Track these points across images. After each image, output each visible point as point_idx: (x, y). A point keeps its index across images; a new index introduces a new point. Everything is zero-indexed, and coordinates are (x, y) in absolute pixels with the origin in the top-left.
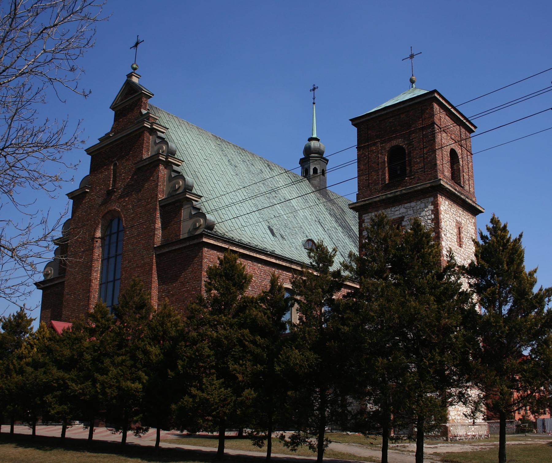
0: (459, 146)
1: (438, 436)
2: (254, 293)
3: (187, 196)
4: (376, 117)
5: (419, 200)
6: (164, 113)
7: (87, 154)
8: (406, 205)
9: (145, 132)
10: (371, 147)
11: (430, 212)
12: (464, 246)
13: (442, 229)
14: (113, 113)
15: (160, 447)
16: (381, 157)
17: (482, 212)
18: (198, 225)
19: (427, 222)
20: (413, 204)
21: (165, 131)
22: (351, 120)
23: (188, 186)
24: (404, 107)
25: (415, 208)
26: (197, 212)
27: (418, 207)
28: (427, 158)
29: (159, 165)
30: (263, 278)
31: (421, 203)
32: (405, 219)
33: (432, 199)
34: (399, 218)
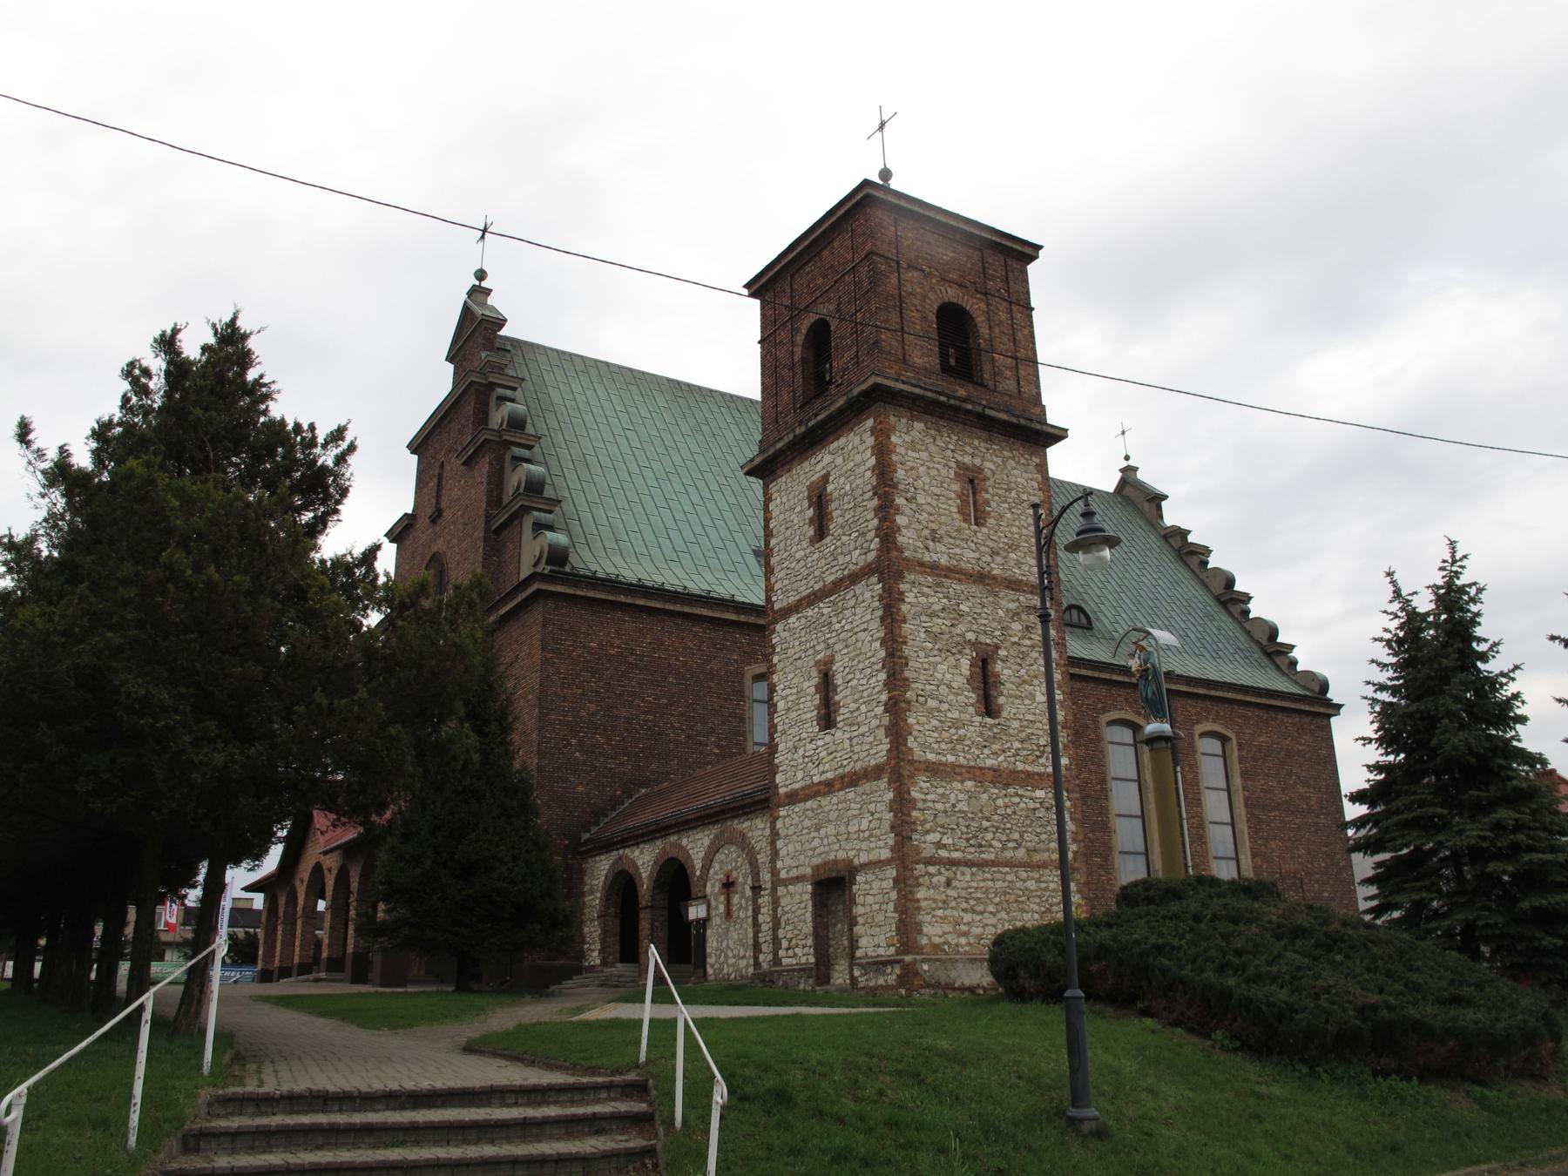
0: (978, 296)
2: (682, 689)
4: (784, 266)
5: (852, 430)
8: (833, 446)
12: (991, 521)
13: (895, 487)
20: (842, 441)
27: (850, 447)
32: (831, 478)
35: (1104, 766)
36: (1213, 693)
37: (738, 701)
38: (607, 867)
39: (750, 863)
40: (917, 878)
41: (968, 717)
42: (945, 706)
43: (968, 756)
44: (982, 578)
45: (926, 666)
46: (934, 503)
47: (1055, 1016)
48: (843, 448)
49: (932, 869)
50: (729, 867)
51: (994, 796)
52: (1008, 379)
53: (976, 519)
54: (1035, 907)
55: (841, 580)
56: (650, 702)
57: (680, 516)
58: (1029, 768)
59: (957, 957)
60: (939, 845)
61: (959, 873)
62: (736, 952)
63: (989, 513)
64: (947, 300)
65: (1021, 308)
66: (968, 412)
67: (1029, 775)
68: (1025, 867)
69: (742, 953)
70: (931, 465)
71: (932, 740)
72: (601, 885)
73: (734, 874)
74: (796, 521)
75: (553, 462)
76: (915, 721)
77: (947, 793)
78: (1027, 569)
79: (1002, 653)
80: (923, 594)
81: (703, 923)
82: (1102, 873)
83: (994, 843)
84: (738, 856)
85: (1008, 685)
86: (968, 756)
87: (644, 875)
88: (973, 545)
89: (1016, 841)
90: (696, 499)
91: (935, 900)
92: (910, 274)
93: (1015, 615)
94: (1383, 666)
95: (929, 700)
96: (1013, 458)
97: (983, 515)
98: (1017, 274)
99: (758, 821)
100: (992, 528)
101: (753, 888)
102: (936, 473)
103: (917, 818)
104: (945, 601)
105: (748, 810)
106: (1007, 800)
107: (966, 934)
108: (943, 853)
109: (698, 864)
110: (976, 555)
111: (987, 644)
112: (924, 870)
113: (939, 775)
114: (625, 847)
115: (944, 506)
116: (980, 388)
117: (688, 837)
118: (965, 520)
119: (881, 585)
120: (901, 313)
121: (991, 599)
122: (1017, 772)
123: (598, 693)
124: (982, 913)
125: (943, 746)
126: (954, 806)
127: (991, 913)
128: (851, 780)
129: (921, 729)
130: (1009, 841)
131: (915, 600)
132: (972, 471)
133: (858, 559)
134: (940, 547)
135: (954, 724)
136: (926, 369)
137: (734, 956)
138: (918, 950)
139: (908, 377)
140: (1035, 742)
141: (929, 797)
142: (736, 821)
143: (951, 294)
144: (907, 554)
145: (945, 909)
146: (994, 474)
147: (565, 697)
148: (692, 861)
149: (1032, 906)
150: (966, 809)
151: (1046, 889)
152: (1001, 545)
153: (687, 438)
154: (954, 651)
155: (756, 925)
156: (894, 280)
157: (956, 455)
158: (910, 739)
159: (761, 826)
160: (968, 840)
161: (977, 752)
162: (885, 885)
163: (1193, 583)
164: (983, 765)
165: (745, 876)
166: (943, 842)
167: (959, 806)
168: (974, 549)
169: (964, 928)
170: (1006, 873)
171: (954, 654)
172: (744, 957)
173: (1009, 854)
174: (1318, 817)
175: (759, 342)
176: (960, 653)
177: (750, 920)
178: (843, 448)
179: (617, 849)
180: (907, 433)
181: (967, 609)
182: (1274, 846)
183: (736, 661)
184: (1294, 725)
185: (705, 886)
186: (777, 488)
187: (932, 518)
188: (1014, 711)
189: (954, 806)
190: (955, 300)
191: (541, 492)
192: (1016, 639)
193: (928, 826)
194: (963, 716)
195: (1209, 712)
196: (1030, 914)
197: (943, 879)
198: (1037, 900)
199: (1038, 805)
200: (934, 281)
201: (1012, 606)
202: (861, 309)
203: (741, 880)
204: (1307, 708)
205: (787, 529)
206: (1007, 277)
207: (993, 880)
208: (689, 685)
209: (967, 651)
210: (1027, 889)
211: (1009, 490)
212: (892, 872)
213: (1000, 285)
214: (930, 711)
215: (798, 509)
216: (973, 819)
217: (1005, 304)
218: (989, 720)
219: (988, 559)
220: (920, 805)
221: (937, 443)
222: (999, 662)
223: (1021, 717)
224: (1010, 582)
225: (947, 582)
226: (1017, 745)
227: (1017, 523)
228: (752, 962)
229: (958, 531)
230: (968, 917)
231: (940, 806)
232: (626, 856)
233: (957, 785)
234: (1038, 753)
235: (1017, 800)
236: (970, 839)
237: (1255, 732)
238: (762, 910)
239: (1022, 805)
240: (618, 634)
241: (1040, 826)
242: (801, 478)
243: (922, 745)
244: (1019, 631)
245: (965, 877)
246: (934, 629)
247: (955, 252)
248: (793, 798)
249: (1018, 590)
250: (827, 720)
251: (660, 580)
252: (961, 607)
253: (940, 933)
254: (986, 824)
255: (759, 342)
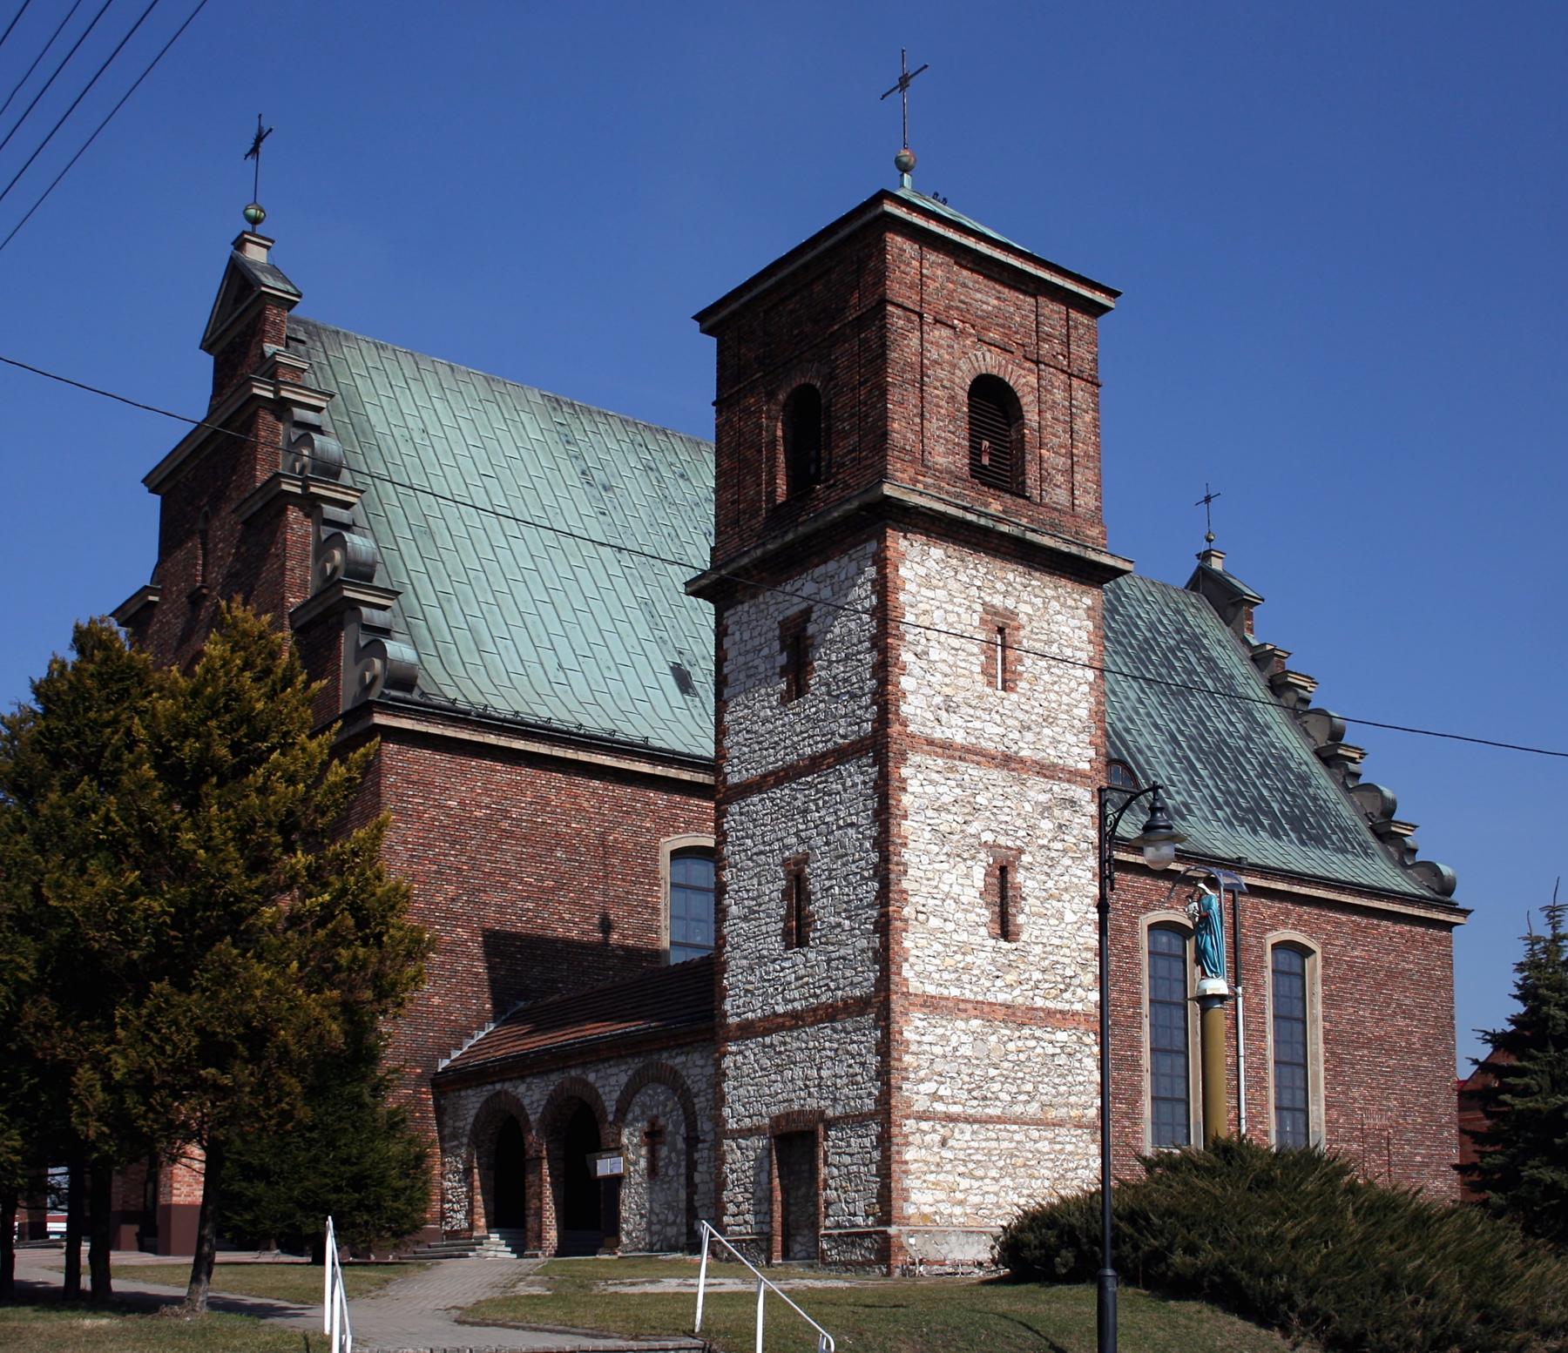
0: (1028, 365)
1: (868, 1263)
3: (346, 593)
4: (755, 298)
5: (844, 552)
6: (363, 344)
7: (151, 491)
9: (262, 413)
10: (745, 397)
11: (869, 586)
12: (1023, 685)
14: (209, 360)
15: (21, 1282)
16: (768, 426)
17: (1123, 572)
18: (368, 675)
19: (860, 619)
20: (831, 566)
21: (323, 404)
22: (698, 317)
23: (357, 563)
24: (817, 257)
25: (836, 579)
26: (371, 638)
27: (843, 577)
28: (867, 416)
29: (287, 509)
30: (611, 822)
31: (851, 560)
32: (814, 616)
33: (872, 546)
34: (802, 612)
35: (1139, 983)
36: (1296, 889)
37: (649, 884)
38: (478, 1105)
39: (685, 1110)
40: (906, 1136)
41: (979, 940)
42: (950, 926)
43: (975, 989)
44: (1007, 761)
45: (930, 875)
46: (951, 660)
47: (1088, 1292)
48: (832, 577)
49: (925, 1125)
50: (655, 1112)
51: (1005, 1039)
52: (1059, 487)
53: (1004, 681)
54: (1047, 1173)
55: (824, 755)
56: (531, 884)
57: (567, 615)
58: (1051, 1005)
59: (951, 1229)
60: (934, 1096)
61: (957, 1130)
62: (662, 1217)
63: (1021, 674)
64: (984, 372)
65: (1083, 384)
66: (1003, 534)
67: (1050, 1013)
68: (1038, 1124)
69: (671, 1218)
70: (949, 607)
71: (932, 968)
72: (468, 1127)
73: (662, 1121)
74: (761, 669)
75: (382, 528)
76: (912, 945)
77: (948, 1033)
78: (1064, 749)
79: (1026, 858)
80: (931, 782)
81: (616, 1181)
82: (1127, 1124)
83: (1002, 1096)
84: (667, 1099)
85: (1031, 900)
86: (975, 989)
87: (532, 1118)
88: (997, 718)
89: (1028, 1093)
90: (590, 591)
91: (926, 1163)
92: (937, 333)
93: (1046, 810)
94: (1316, 1146)
95: (931, 918)
96: (1057, 598)
97: (1013, 677)
98: (1081, 331)
99: (696, 1056)
100: (1024, 694)
101: (687, 1140)
102: (956, 619)
103: (910, 1064)
104: (958, 790)
105: (680, 1041)
106: (1020, 1043)
107: (961, 1203)
108: (940, 1107)
109: (611, 1106)
110: (1001, 730)
111: (1008, 848)
112: (915, 1126)
113: (939, 1011)
114: (503, 1081)
115: (963, 664)
116: (1021, 501)
117: (597, 1071)
118: (990, 684)
119: (877, 768)
120: (922, 390)
121: (1016, 789)
122: (1036, 1009)
123: (459, 870)
124: (982, 1179)
125: (946, 976)
126: (955, 1049)
127: (994, 1178)
128: (830, 1014)
129: (920, 954)
130: (1019, 1093)
131: (920, 789)
132: (1003, 616)
133: (843, 731)
134: (955, 719)
135: (960, 948)
136: (951, 472)
137: (659, 1222)
138: (905, 1221)
139: (926, 486)
140: (1061, 972)
141: (926, 1039)
142: (665, 1055)
143: (990, 362)
144: (911, 728)
145: (938, 1173)
146: (1031, 621)
147: (414, 875)
148: (602, 1103)
149: (1043, 1171)
150: (969, 1053)
151: (1061, 1151)
152: (1034, 717)
153: (574, 492)
154: (965, 855)
155: (691, 1186)
156: (915, 342)
157: (982, 594)
158: (906, 966)
159: (700, 1062)
160: (970, 1091)
161: (988, 984)
162: (867, 1142)
163: (1285, 729)
164: (994, 1001)
165: (676, 1125)
166: (940, 1093)
167: (962, 1051)
168: (999, 722)
169: (959, 1196)
170: (1015, 1132)
171: (965, 860)
172: (674, 1223)
173: (1018, 1109)
174: (1420, 1059)
175: (714, 404)
176: (973, 858)
177: (682, 1180)
178: (832, 577)
179: (493, 1083)
180: (921, 564)
181: (985, 802)
182: (1357, 1095)
183: (648, 830)
184: (1402, 935)
185: (619, 1134)
186: (736, 618)
187: (947, 680)
188: (1036, 933)
189: (955, 1049)
190: (995, 372)
191: (370, 578)
192: (1045, 842)
193: (922, 1074)
194: (972, 939)
195: (1288, 914)
196: (1039, 1181)
197: (937, 1138)
198: (1050, 1164)
199: (1058, 1051)
200: (968, 342)
201: (1043, 798)
202: (866, 381)
203: (670, 1128)
204: (1422, 913)
205: (748, 677)
206: (1068, 336)
207: (997, 1139)
208: (583, 862)
209: (982, 856)
210: (1039, 1152)
211: (1050, 642)
212: (875, 1129)
213: (1058, 348)
214: (932, 932)
215: (765, 652)
216: (978, 1066)
217: (1063, 377)
218: (1003, 944)
219: (1016, 735)
220: (914, 1048)
221: (959, 577)
222: (1021, 870)
223: (1044, 941)
224: (1042, 767)
225: (961, 766)
226: (1037, 976)
227: (1056, 688)
228: (684, 1230)
229: (980, 697)
230: (965, 1183)
231: (938, 1050)
232: (506, 1093)
233: (960, 1024)
234: (1062, 987)
235: (1032, 1043)
236: (973, 1089)
237: (1349, 944)
238: (700, 1168)
239: (1039, 1050)
240: (486, 789)
241: (1059, 1076)
242: (771, 610)
243: (918, 975)
244: (1050, 830)
245: (964, 1135)
246: (942, 828)
247: (998, 298)
248: (748, 1030)
249: (1052, 777)
250: (797, 932)
251: (544, 713)
252: (979, 799)
253: (931, 1201)
254: (992, 1072)
255: (714, 404)
